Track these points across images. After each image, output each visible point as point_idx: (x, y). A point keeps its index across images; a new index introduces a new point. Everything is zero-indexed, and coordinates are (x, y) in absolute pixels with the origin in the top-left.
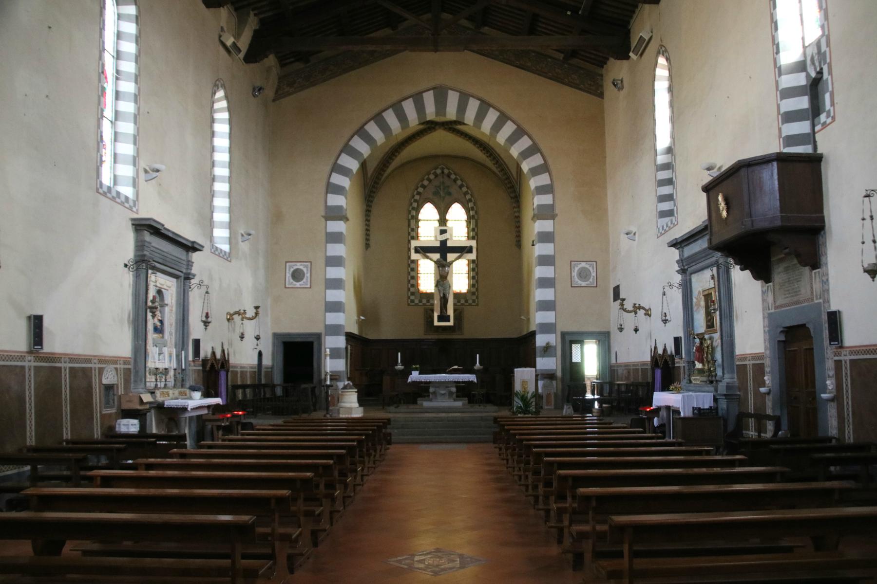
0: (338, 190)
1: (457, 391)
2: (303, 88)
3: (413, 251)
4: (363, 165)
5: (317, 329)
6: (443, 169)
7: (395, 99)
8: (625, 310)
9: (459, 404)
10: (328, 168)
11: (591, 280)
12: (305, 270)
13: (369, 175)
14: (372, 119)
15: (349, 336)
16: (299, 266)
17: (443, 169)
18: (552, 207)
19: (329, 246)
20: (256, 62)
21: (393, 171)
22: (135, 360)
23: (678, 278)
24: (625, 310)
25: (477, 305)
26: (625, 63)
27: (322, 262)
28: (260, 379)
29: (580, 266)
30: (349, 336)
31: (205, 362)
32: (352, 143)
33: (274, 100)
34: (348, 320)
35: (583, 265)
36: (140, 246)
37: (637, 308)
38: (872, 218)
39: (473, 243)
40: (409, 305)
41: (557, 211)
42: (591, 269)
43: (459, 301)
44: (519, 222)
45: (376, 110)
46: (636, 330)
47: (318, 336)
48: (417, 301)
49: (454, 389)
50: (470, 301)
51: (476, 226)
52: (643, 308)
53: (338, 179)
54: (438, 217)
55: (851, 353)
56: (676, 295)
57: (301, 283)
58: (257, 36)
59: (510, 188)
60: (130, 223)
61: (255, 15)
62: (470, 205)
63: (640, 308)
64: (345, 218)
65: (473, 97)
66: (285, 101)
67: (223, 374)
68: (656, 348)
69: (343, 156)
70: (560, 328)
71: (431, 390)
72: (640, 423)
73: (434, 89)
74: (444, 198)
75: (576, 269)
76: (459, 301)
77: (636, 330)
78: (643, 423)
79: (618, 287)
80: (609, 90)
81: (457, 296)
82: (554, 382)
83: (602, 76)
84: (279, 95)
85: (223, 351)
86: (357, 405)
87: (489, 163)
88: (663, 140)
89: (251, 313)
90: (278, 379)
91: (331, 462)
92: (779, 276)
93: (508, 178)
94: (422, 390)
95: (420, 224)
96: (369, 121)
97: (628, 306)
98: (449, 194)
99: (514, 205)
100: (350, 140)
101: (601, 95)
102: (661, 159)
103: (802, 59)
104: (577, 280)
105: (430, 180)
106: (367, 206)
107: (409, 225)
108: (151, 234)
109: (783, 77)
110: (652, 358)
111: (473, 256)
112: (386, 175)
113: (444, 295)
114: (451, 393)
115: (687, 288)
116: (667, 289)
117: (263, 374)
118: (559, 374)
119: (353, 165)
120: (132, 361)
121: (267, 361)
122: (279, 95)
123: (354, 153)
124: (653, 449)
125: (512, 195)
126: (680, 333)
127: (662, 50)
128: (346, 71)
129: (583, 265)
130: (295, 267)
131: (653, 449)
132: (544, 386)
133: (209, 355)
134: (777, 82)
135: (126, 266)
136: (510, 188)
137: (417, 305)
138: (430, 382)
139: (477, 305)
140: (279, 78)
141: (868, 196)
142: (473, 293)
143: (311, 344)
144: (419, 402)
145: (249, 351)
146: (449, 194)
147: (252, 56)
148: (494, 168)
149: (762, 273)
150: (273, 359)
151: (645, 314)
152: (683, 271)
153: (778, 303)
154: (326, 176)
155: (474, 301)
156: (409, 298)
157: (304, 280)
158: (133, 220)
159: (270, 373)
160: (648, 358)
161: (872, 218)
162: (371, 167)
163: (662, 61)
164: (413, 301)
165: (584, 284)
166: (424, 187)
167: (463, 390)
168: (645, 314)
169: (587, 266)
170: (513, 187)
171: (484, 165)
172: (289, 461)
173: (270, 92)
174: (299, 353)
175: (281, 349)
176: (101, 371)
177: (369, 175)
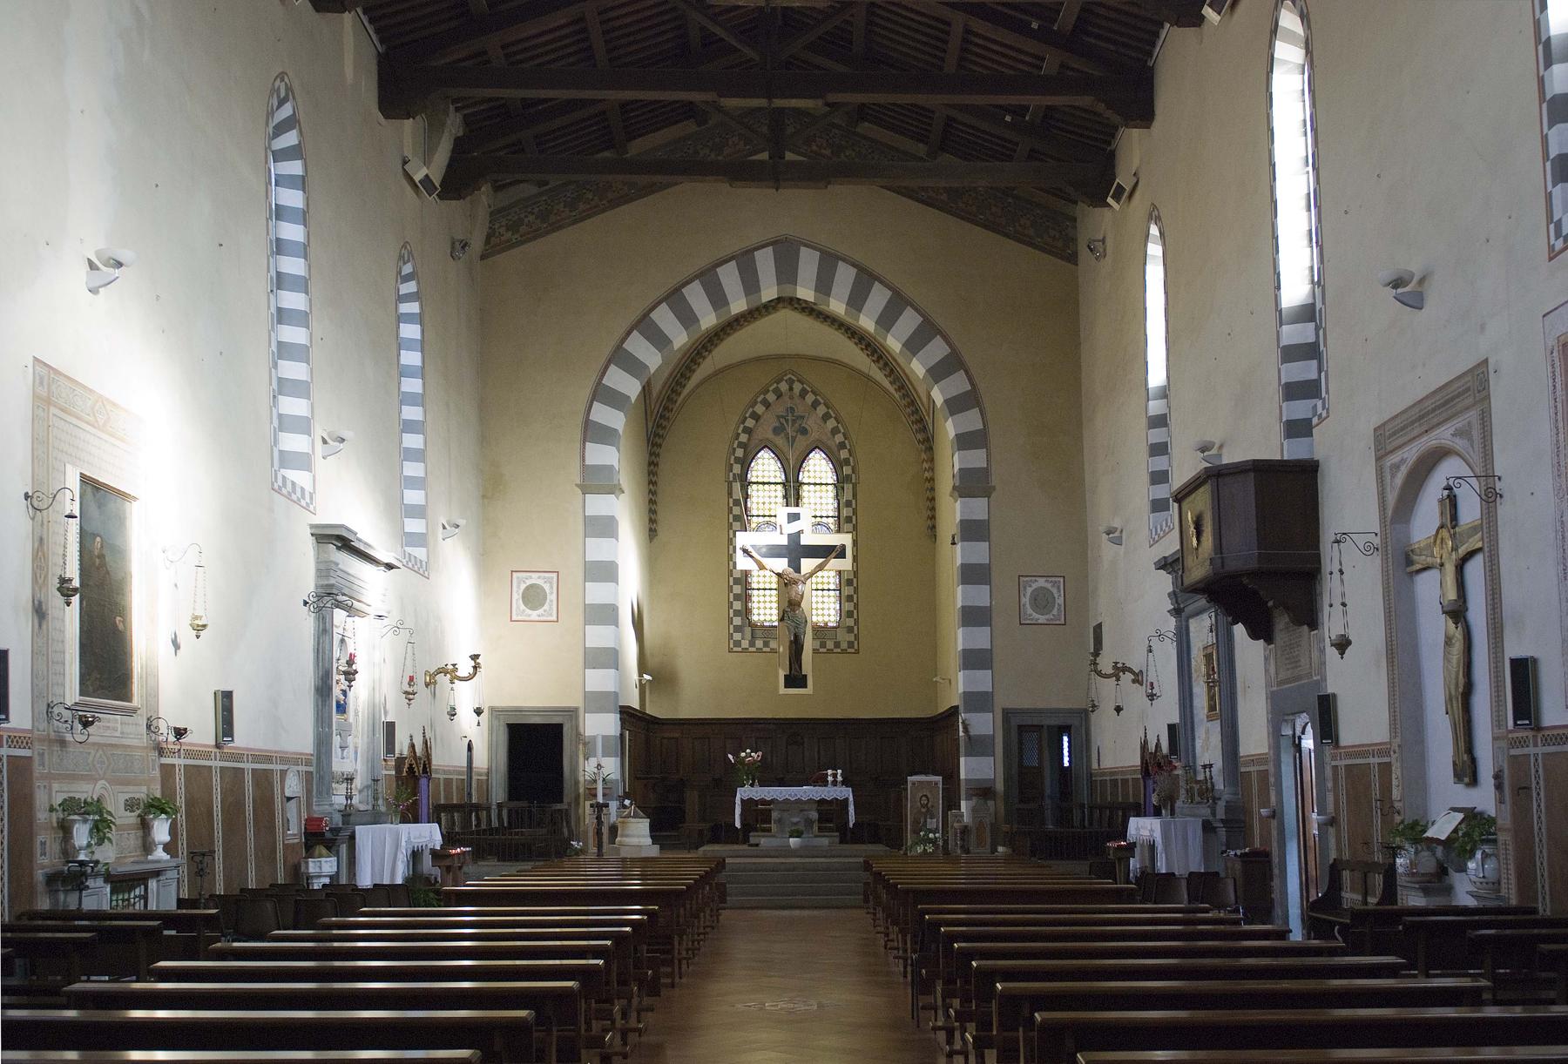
0: (603, 435)
1: (820, 820)
2: (535, 235)
3: (739, 553)
4: (646, 390)
5: (573, 700)
6: (791, 382)
7: (702, 262)
8: (1099, 673)
9: (825, 841)
10: (586, 393)
11: (1055, 612)
12: (546, 587)
13: (655, 394)
14: (665, 299)
15: (627, 714)
16: (535, 579)
17: (791, 382)
18: (984, 473)
19: (591, 542)
20: (459, 197)
21: (697, 386)
22: (319, 758)
23: (1172, 622)
24: (1099, 673)
25: (857, 652)
26: (1190, 32)
27: (579, 573)
28: (470, 794)
29: (1035, 586)
30: (627, 714)
31: (400, 761)
32: (627, 346)
33: (483, 257)
34: (628, 682)
35: (1041, 582)
36: (324, 569)
37: (1120, 669)
38: (1341, 572)
39: (845, 539)
40: (730, 651)
41: (995, 480)
42: (1055, 591)
43: (823, 645)
44: (933, 489)
45: (672, 283)
46: (1118, 709)
47: (572, 713)
48: (745, 644)
49: (814, 815)
50: (844, 645)
51: (855, 496)
52: (1130, 670)
53: (605, 415)
54: (781, 477)
55: (1350, 755)
56: (1167, 653)
57: (541, 611)
58: (459, 146)
59: (917, 422)
60: (309, 531)
61: (457, 110)
62: (844, 454)
63: (1125, 669)
64: (614, 489)
65: (844, 260)
66: (501, 259)
67: (423, 781)
68: (1146, 742)
69: (613, 369)
70: (1001, 702)
71: (775, 815)
72: (1108, 870)
73: (774, 243)
74: (794, 439)
75: (1029, 590)
76: (823, 645)
77: (1118, 709)
78: (1111, 866)
79: (1100, 626)
80: (1084, 253)
81: (821, 631)
82: (991, 803)
83: (1075, 220)
84: (493, 247)
85: (425, 742)
86: (649, 841)
87: (878, 375)
88: (1157, 376)
89: (465, 668)
90: (499, 794)
91: (609, 943)
92: (1280, 636)
93: (913, 403)
94: (758, 814)
95: (753, 490)
96: (659, 303)
97: (1105, 665)
98: (804, 431)
99: (924, 456)
100: (623, 340)
101: (1073, 259)
102: (1156, 407)
103: (1310, 301)
104: (1030, 611)
105: (767, 405)
106: (651, 454)
107: (730, 494)
108: (339, 548)
109: (1557, 69)
110: (1143, 758)
111: (846, 564)
112: (686, 391)
113: (796, 636)
114: (809, 823)
115: (1183, 639)
116: (1155, 643)
117: (474, 785)
118: (1000, 787)
119: (631, 387)
120: (314, 759)
121: (481, 760)
122: (493, 247)
123: (632, 365)
124: (1286, 985)
125: (920, 437)
126: (1176, 719)
127: (1154, 216)
128: (614, 204)
129: (1041, 582)
130: (529, 582)
131: (1286, 985)
132: (974, 810)
133: (406, 753)
134: (1541, 81)
135: (306, 603)
136: (917, 422)
137: (745, 650)
138: (772, 801)
139: (857, 652)
140: (491, 214)
141: (1338, 542)
142: (850, 630)
143: (559, 727)
144: (752, 840)
145: (468, 738)
146: (804, 431)
147: (455, 185)
148: (886, 383)
149: (1261, 630)
150: (490, 760)
151: (1134, 681)
152: (1177, 612)
153: (1282, 676)
154: (582, 408)
155: (851, 644)
156: (731, 636)
157: (546, 607)
158: (312, 526)
159: (485, 787)
160: (1136, 761)
161: (1341, 572)
162: (657, 388)
163: (1289, 20)
164: (738, 643)
165: (1042, 619)
166: (756, 417)
167: (830, 813)
168: (1134, 681)
169: (1049, 586)
170: (921, 420)
171: (869, 378)
172: (518, 962)
173: (477, 244)
174: (535, 745)
175: (503, 737)
176: (283, 773)
177: (655, 394)
